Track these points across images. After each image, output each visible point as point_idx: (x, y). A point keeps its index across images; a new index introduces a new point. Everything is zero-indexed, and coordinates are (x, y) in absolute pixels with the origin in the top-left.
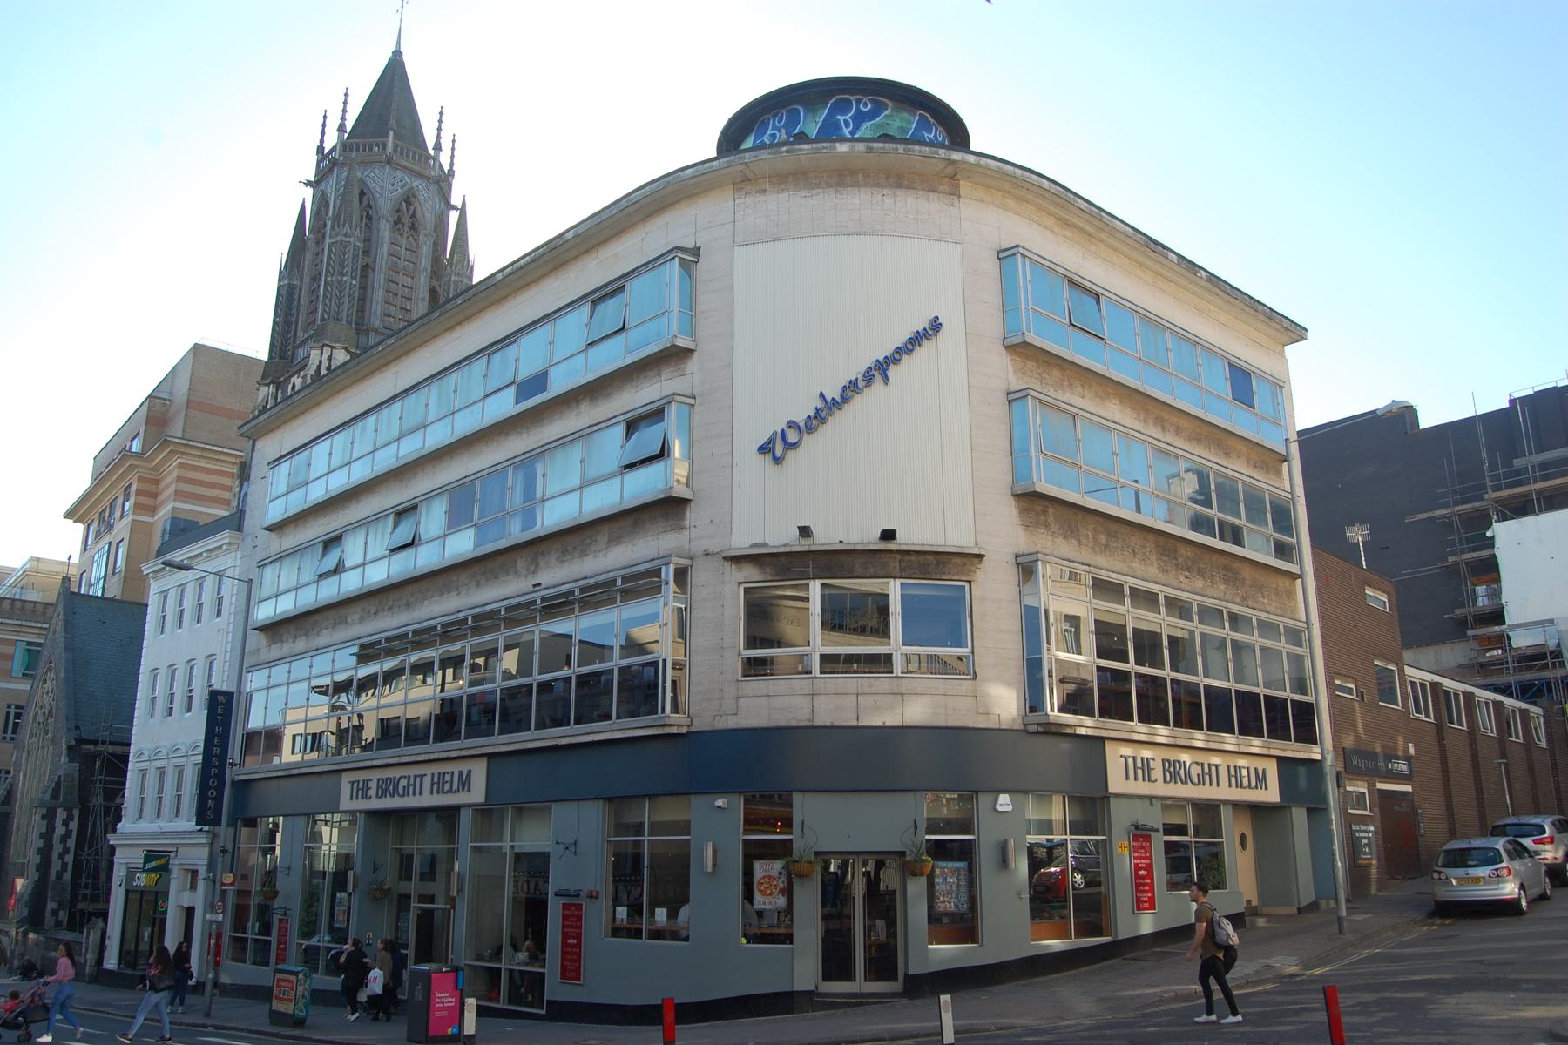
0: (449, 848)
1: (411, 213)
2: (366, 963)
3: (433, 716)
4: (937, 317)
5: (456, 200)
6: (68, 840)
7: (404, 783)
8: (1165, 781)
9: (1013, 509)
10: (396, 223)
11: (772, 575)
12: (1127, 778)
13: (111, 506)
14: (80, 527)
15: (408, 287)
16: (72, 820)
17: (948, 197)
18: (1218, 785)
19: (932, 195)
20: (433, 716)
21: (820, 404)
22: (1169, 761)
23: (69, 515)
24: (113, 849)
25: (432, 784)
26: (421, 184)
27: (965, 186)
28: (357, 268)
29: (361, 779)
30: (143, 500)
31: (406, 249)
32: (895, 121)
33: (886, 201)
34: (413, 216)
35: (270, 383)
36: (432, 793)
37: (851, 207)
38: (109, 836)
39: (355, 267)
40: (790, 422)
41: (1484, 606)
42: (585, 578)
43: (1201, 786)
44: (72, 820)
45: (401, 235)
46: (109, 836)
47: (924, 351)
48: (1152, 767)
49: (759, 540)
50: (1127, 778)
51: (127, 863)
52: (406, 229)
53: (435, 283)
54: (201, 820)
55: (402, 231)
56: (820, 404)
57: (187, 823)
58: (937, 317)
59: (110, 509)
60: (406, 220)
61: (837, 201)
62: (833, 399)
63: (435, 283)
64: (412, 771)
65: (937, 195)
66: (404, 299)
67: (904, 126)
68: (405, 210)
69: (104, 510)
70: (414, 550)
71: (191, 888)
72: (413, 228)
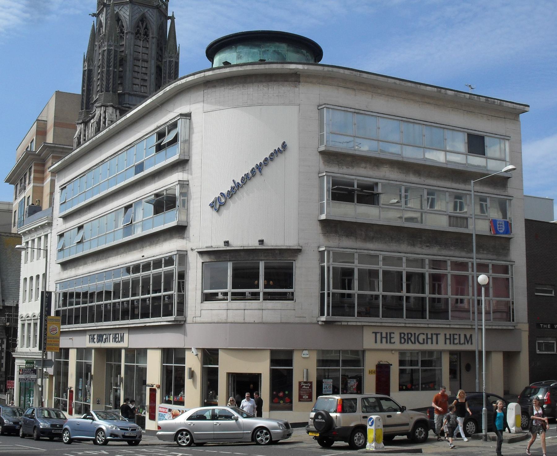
0: (138, 363)
1: (144, 27)
2: (448, 427)
3: (486, 212)
4: (284, 142)
5: (170, 14)
6: (3, 353)
7: (104, 337)
8: (401, 342)
9: (319, 226)
10: (136, 34)
11: (214, 259)
12: (376, 342)
13: (24, 177)
14: (13, 186)
15: (145, 67)
16: (4, 344)
17: (293, 83)
18: (437, 343)
19: (286, 83)
20: (486, 212)
21: (233, 185)
22: (404, 334)
23: (8, 181)
24: (14, 359)
25: (113, 338)
26: (149, 10)
27: (301, 79)
28: (117, 63)
29: (92, 334)
30: (38, 175)
31: (143, 47)
32: (272, 48)
33: (264, 89)
34: (146, 28)
35: (101, 106)
36: (113, 342)
37: (249, 93)
38: (13, 353)
39: (115, 62)
40: (221, 193)
41: (12, 355)
42: (154, 256)
43: (425, 344)
44: (4, 344)
45: (140, 40)
46: (13, 353)
47: (280, 160)
48: (392, 336)
49: (210, 245)
50: (376, 342)
51: (19, 366)
52: (142, 36)
53: (159, 63)
54: (40, 349)
55: (140, 38)
56: (233, 185)
57: (37, 349)
58: (284, 142)
59: (24, 178)
60: (142, 31)
61: (243, 90)
62: (238, 183)
63: (159, 63)
64: (107, 333)
65: (288, 83)
66: (143, 74)
67: (276, 49)
68: (141, 26)
69: (22, 178)
70: (82, 244)
71: (323, 361)
72: (146, 34)
